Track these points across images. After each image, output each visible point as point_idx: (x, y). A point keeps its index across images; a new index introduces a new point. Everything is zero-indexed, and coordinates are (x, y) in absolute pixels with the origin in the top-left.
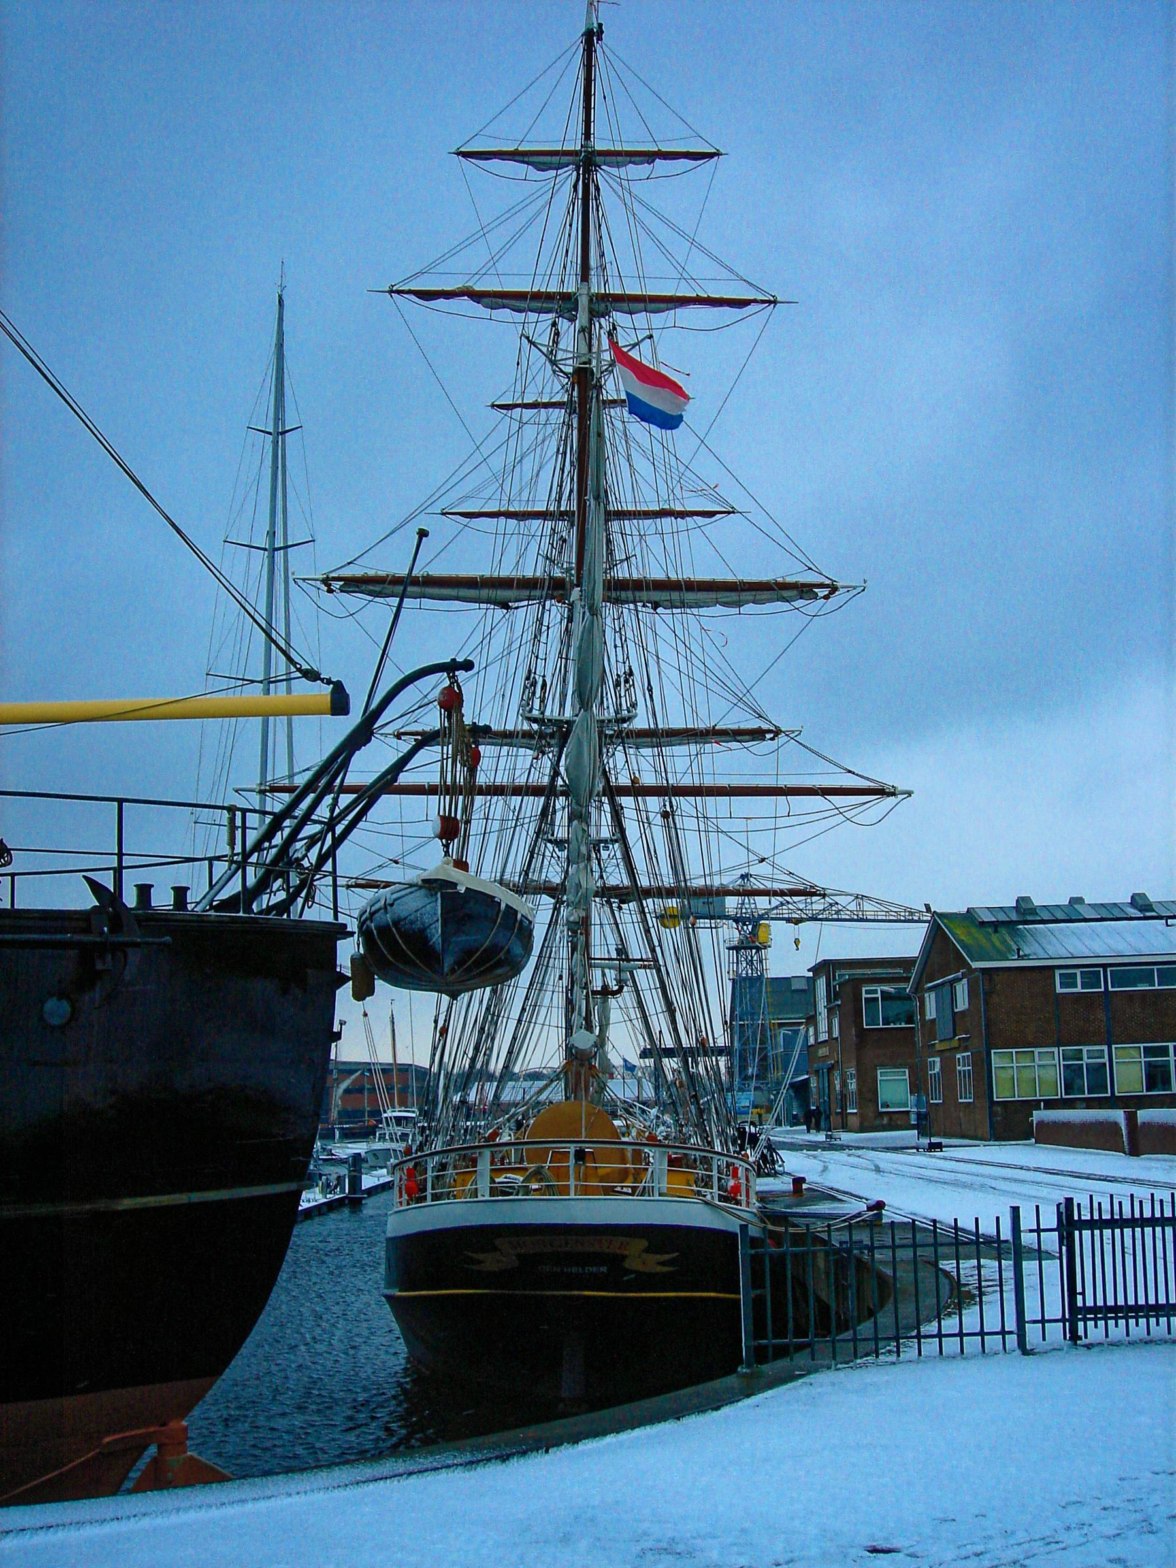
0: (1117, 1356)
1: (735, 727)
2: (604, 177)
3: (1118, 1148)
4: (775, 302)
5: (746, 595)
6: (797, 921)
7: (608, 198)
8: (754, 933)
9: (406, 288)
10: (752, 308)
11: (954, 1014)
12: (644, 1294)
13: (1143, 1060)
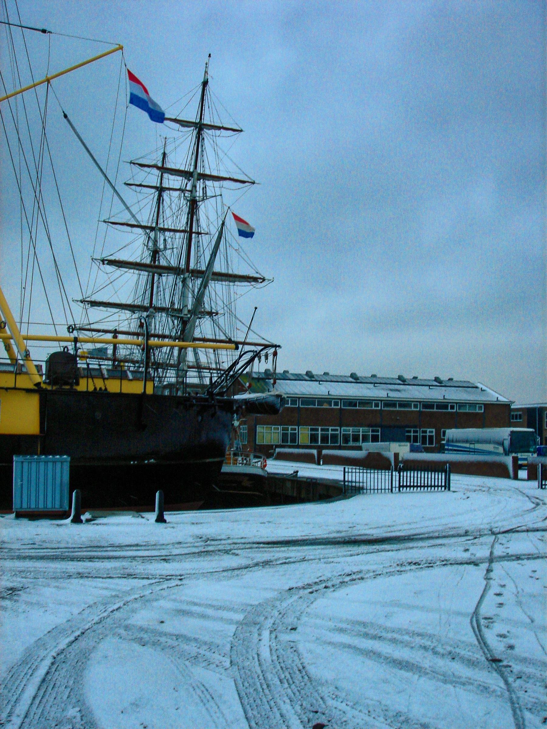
0: (407, 494)
2: (207, 134)
4: (253, 183)
5: (237, 279)
7: (207, 143)
9: (136, 162)
10: (247, 184)
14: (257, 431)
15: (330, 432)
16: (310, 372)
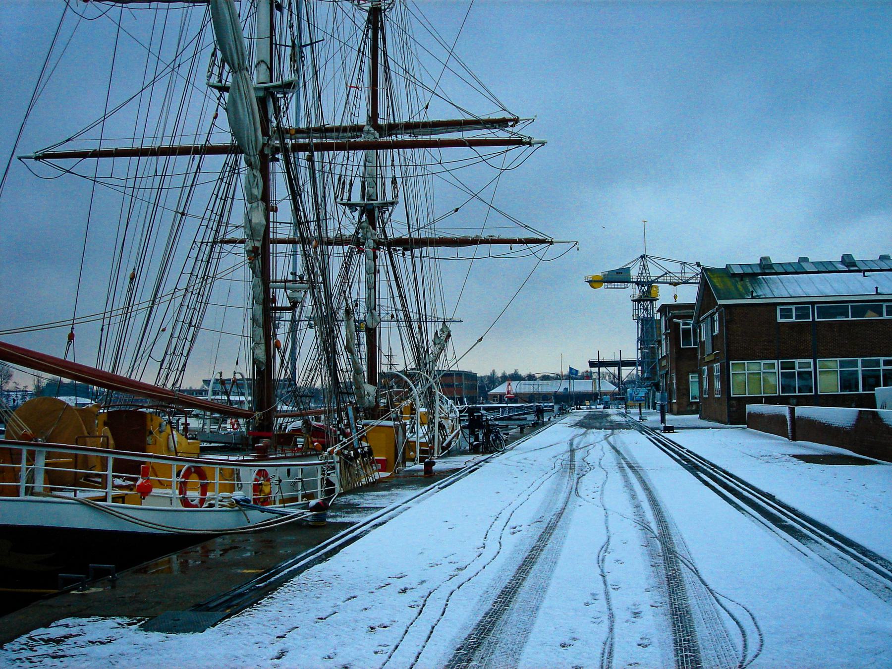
1: (486, 118)
3: (786, 436)
6: (676, 284)
8: (648, 291)
11: (712, 336)
12: (34, 591)
13: (839, 369)
14: (731, 373)
15: (882, 367)
16: (849, 256)
